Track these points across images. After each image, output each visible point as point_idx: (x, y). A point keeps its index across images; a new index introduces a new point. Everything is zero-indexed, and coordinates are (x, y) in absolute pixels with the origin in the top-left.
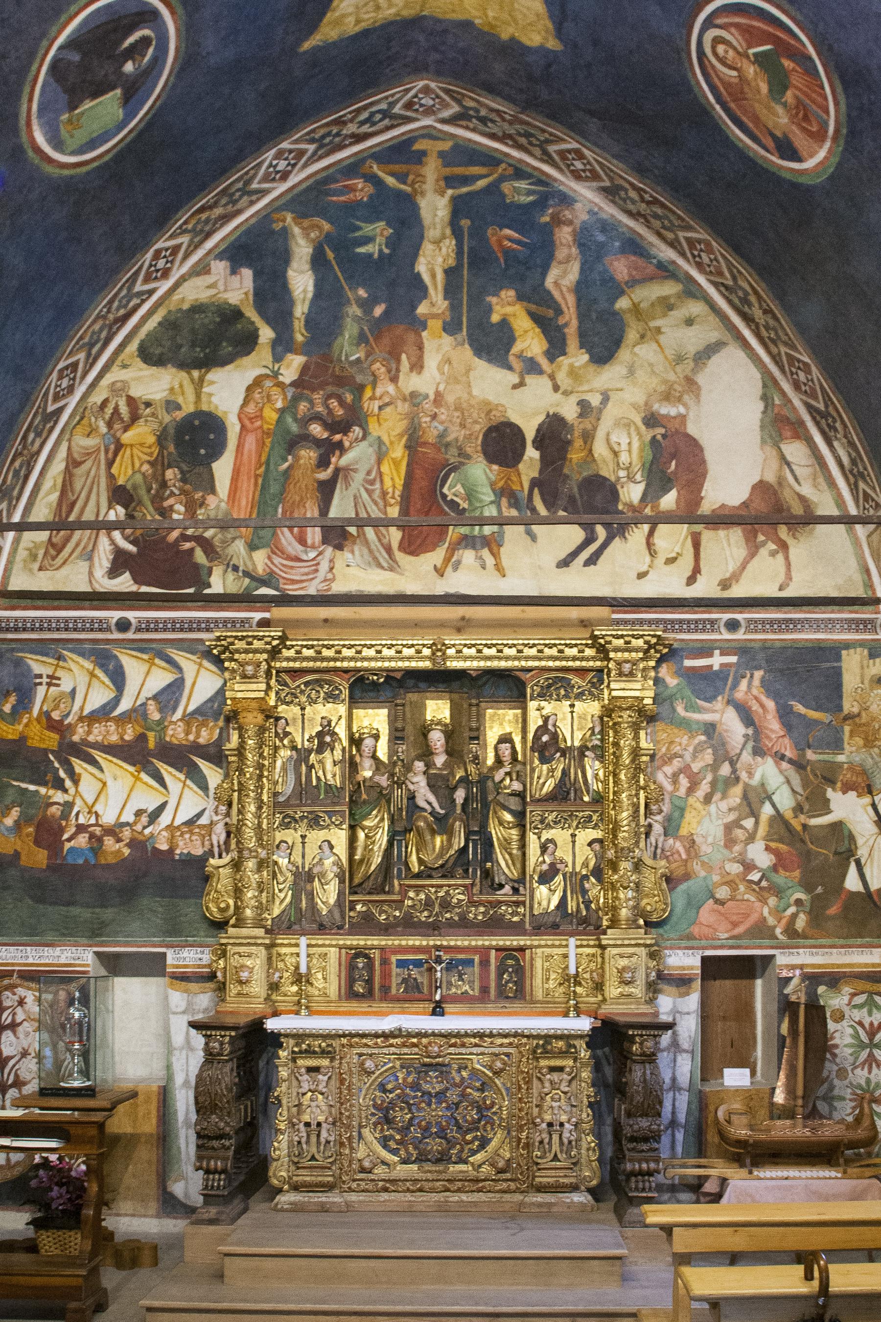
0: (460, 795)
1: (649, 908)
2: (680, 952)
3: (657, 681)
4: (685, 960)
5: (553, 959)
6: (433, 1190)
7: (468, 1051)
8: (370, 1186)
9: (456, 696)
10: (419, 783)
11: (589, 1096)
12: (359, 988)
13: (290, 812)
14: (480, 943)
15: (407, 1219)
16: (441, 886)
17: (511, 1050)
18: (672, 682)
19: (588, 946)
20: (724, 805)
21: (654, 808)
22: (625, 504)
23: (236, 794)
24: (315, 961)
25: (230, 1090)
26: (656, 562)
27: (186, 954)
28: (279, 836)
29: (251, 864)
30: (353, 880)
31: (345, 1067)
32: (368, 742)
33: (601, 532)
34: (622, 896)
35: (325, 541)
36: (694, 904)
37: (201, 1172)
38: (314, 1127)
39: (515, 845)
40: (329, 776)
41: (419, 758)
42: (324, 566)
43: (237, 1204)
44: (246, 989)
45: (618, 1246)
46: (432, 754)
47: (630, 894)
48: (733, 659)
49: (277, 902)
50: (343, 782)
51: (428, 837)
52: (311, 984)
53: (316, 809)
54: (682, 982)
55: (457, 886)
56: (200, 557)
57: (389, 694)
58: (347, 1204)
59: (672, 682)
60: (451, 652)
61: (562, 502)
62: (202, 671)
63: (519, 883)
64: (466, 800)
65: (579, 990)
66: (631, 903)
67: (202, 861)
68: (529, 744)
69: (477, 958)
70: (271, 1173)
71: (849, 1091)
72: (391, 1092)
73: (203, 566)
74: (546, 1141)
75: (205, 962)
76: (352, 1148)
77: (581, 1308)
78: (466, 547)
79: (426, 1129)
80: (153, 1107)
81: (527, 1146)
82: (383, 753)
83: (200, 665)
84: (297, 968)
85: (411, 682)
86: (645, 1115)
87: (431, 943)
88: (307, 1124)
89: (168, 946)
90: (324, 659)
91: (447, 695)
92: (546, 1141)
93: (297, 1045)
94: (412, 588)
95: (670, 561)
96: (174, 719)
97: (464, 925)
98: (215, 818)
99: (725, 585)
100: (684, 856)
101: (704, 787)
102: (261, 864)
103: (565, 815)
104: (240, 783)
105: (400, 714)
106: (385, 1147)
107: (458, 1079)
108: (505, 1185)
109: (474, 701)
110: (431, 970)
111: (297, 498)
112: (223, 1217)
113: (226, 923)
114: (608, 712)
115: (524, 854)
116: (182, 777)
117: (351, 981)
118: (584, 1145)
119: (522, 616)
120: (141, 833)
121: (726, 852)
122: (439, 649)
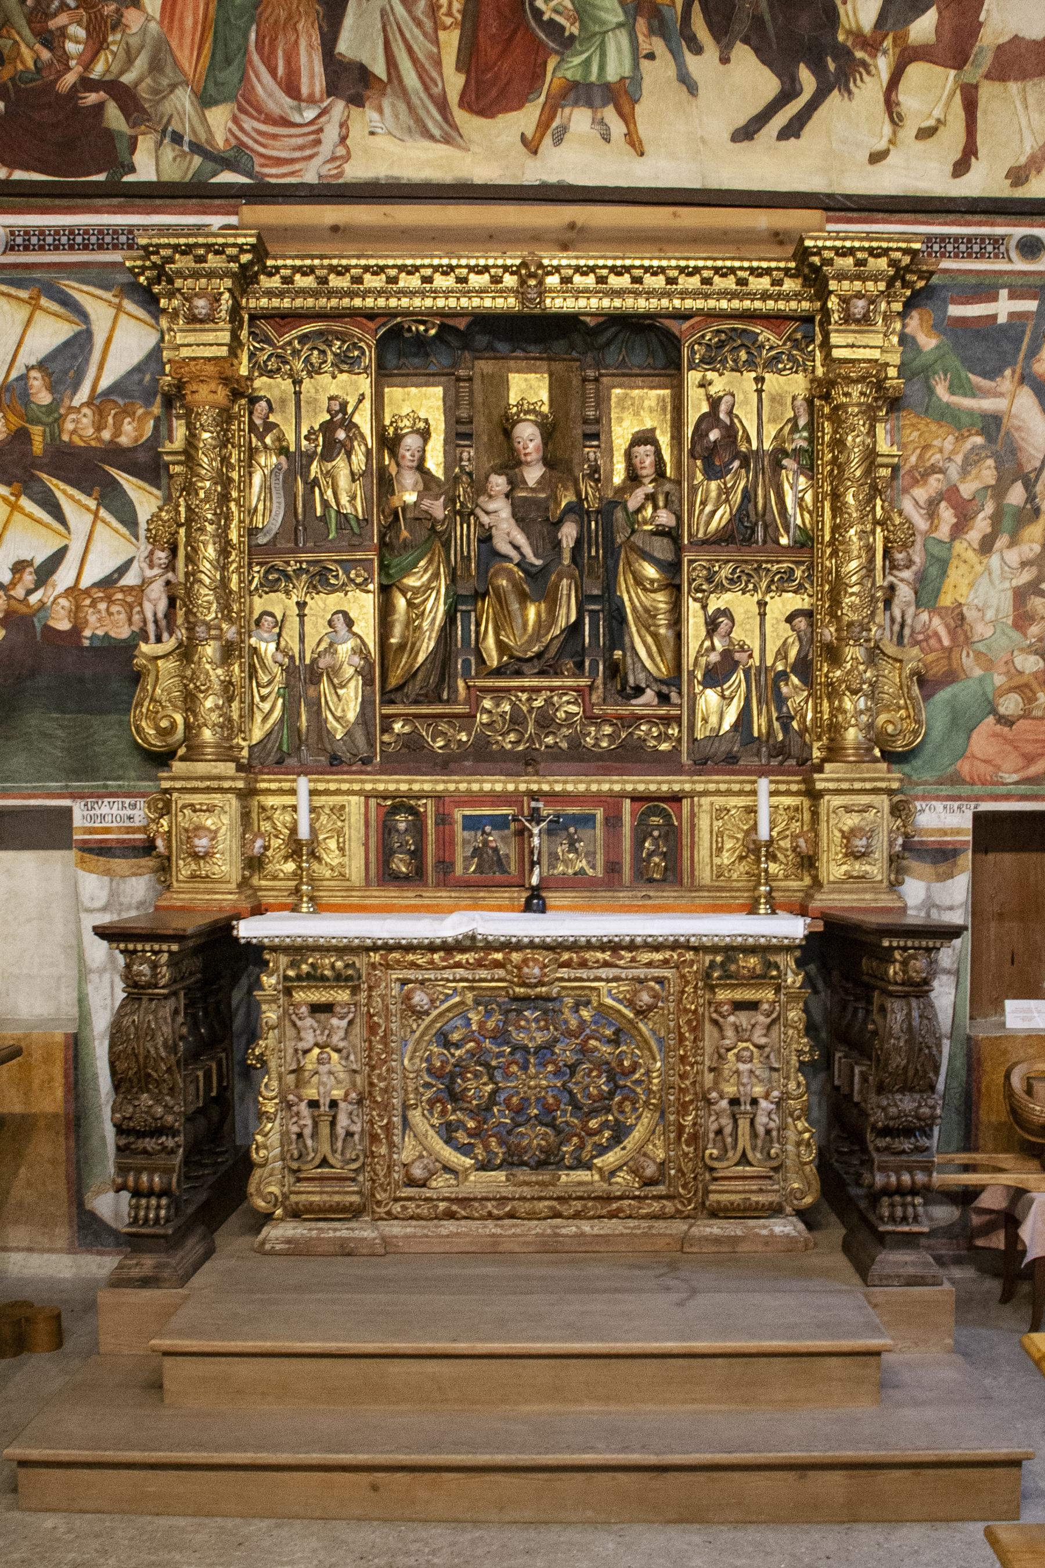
0: (568, 533)
1: (890, 728)
2: (939, 805)
3: (904, 339)
4: (945, 819)
5: (732, 815)
6: (532, 1216)
7: (592, 973)
8: (424, 1210)
9: (558, 366)
10: (498, 513)
11: (800, 1052)
12: (400, 865)
13: (278, 563)
14: (605, 787)
15: (491, 1270)
16: (537, 690)
17: (667, 973)
18: (928, 342)
19: (788, 793)
20: (1013, 556)
21: (899, 556)
22: (849, 32)
23: (182, 531)
24: (324, 819)
25: (173, 1049)
26: (901, 134)
27: (105, 810)
28: (259, 604)
29: (210, 650)
30: (388, 677)
31: (378, 1003)
32: (411, 442)
33: (807, 79)
34: (848, 705)
35: (332, 89)
36: (962, 724)
37: (125, 1195)
38: (324, 1108)
39: (662, 620)
40: (344, 499)
41: (499, 470)
42: (331, 134)
43: (193, 1246)
44: (205, 869)
45: (876, 1331)
46: (519, 463)
47: (862, 704)
48: (1031, 305)
49: (258, 717)
50: (368, 510)
51: (515, 606)
52: (319, 859)
53: (323, 556)
54: (942, 856)
55: (565, 690)
56: (114, 117)
57: (445, 361)
58: (385, 1240)
59: (928, 342)
60: (553, 281)
61: (742, 26)
62: (123, 318)
63: (671, 684)
64: (579, 542)
65: (773, 868)
66: (864, 718)
67: (127, 648)
68: (687, 445)
69: (599, 814)
70: (252, 1189)
72: (457, 1046)
73: (121, 134)
74: (728, 1130)
75: (137, 823)
76: (391, 1145)
77: (817, 1454)
78: (576, 103)
79: (520, 1110)
80: (58, 1071)
81: (694, 1139)
82: (435, 463)
83: (119, 308)
84: (294, 830)
85: (481, 340)
86: (907, 1088)
87: (523, 787)
88: (313, 1104)
89: (73, 796)
90: (331, 293)
91: (544, 364)
92: (728, 1130)
93: (293, 965)
94: (483, 172)
95: (926, 133)
96: (76, 403)
97: (578, 756)
98: (149, 573)
99: (1018, 176)
100: (946, 642)
101: (981, 525)
102: (229, 652)
103: (748, 569)
104: (188, 508)
105: (464, 393)
106: (449, 1141)
107: (574, 1023)
108: (656, 1206)
109: (591, 373)
110: (522, 833)
111: (283, 15)
112: (166, 1274)
113: (171, 754)
114: (822, 391)
115: (678, 636)
116: (92, 504)
117: (386, 853)
118: (791, 1135)
119: (677, 223)
120: (24, 601)
121: (1016, 635)
122: (530, 274)
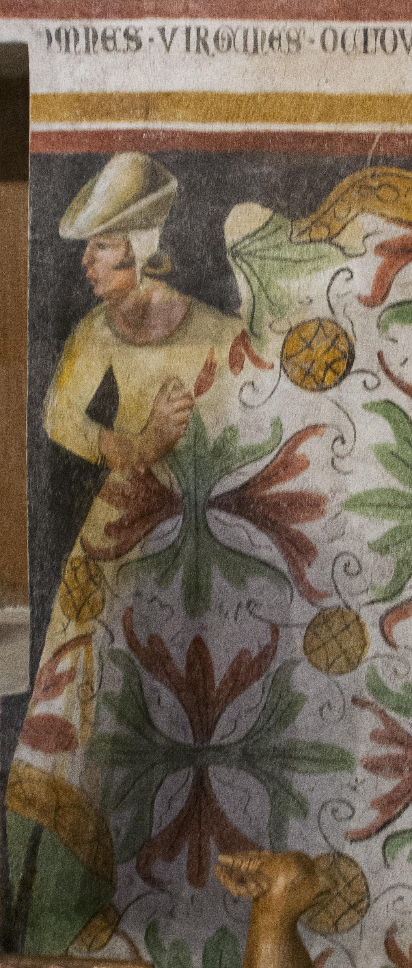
71: (368, 721)
85: (35, 424)
